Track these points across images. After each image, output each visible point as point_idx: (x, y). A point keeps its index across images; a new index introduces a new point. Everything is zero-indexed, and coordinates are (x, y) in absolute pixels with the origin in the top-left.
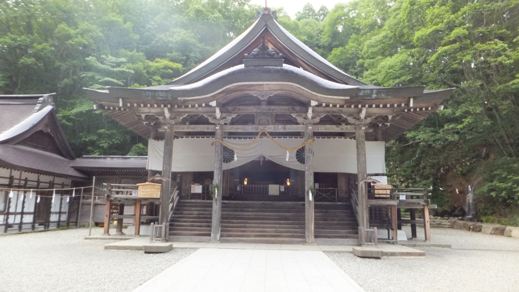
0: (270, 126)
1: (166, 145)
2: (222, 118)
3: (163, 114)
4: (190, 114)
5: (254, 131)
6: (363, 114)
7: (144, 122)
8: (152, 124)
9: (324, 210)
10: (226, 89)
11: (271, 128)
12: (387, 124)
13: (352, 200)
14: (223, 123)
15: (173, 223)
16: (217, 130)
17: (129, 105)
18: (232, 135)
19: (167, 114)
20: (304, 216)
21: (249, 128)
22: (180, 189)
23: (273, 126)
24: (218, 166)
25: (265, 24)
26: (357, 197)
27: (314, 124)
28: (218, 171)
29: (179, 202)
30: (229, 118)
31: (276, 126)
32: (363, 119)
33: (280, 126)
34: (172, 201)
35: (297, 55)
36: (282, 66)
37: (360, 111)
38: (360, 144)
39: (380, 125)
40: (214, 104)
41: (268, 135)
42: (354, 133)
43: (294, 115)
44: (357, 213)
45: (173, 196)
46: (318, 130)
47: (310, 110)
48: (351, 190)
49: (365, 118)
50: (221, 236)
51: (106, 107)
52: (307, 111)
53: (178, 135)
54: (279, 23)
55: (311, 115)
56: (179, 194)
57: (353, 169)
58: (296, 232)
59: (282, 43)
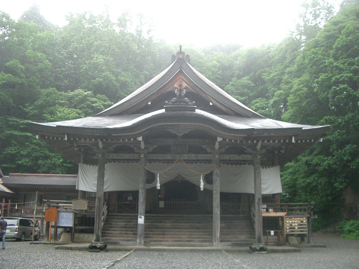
0: (185, 155)
1: (100, 170)
2: (145, 148)
3: (97, 145)
4: (118, 145)
5: (171, 158)
6: (259, 147)
7: (76, 149)
8: (82, 150)
9: (229, 221)
10: (151, 128)
11: (186, 156)
12: (281, 151)
13: (251, 213)
14: (146, 153)
15: (104, 231)
16: (141, 158)
17: (72, 139)
18: (150, 161)
19: (101, 145)
20: (212, 225)
21: (168, 157)
22: (108, 204)
23: (187, 155)
24: (142, 187)
25: (180, 66)
26: (255, 211)
27: (220, 154)
28: (142, 190)
29: (107, 215)
30: (151, 148)
31: (190, 155)
32: (259, 150)
33: (193, 155)
34: (103, 215)
35: (208, 93)
36: (195, 111)
37: (257, 144)
38: (257, 170)
39: (276, 152)
40: (140, 139)
41: (183, 161)
42: (253, 160)
43: (204, 147)
44: (254, 222)
45: (104, 211)
46: (224, 158)
47: (217, 144)
48: (251, 205)
49: (261, 149)
50: (145, 242)
51: (46, 137)
52: (215, 144)
53: (110, 161)
54: (191, 65)
55: (218, 147)
56: (108, 209)
57: (251, 191)
58: (205, 238)
59: (194, 82)
